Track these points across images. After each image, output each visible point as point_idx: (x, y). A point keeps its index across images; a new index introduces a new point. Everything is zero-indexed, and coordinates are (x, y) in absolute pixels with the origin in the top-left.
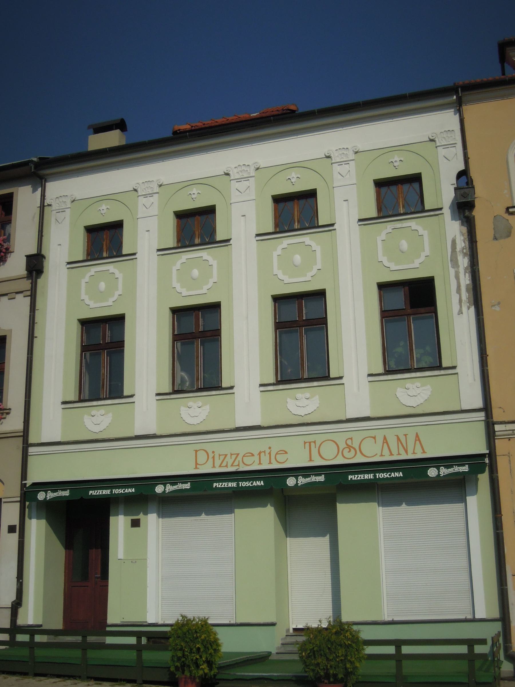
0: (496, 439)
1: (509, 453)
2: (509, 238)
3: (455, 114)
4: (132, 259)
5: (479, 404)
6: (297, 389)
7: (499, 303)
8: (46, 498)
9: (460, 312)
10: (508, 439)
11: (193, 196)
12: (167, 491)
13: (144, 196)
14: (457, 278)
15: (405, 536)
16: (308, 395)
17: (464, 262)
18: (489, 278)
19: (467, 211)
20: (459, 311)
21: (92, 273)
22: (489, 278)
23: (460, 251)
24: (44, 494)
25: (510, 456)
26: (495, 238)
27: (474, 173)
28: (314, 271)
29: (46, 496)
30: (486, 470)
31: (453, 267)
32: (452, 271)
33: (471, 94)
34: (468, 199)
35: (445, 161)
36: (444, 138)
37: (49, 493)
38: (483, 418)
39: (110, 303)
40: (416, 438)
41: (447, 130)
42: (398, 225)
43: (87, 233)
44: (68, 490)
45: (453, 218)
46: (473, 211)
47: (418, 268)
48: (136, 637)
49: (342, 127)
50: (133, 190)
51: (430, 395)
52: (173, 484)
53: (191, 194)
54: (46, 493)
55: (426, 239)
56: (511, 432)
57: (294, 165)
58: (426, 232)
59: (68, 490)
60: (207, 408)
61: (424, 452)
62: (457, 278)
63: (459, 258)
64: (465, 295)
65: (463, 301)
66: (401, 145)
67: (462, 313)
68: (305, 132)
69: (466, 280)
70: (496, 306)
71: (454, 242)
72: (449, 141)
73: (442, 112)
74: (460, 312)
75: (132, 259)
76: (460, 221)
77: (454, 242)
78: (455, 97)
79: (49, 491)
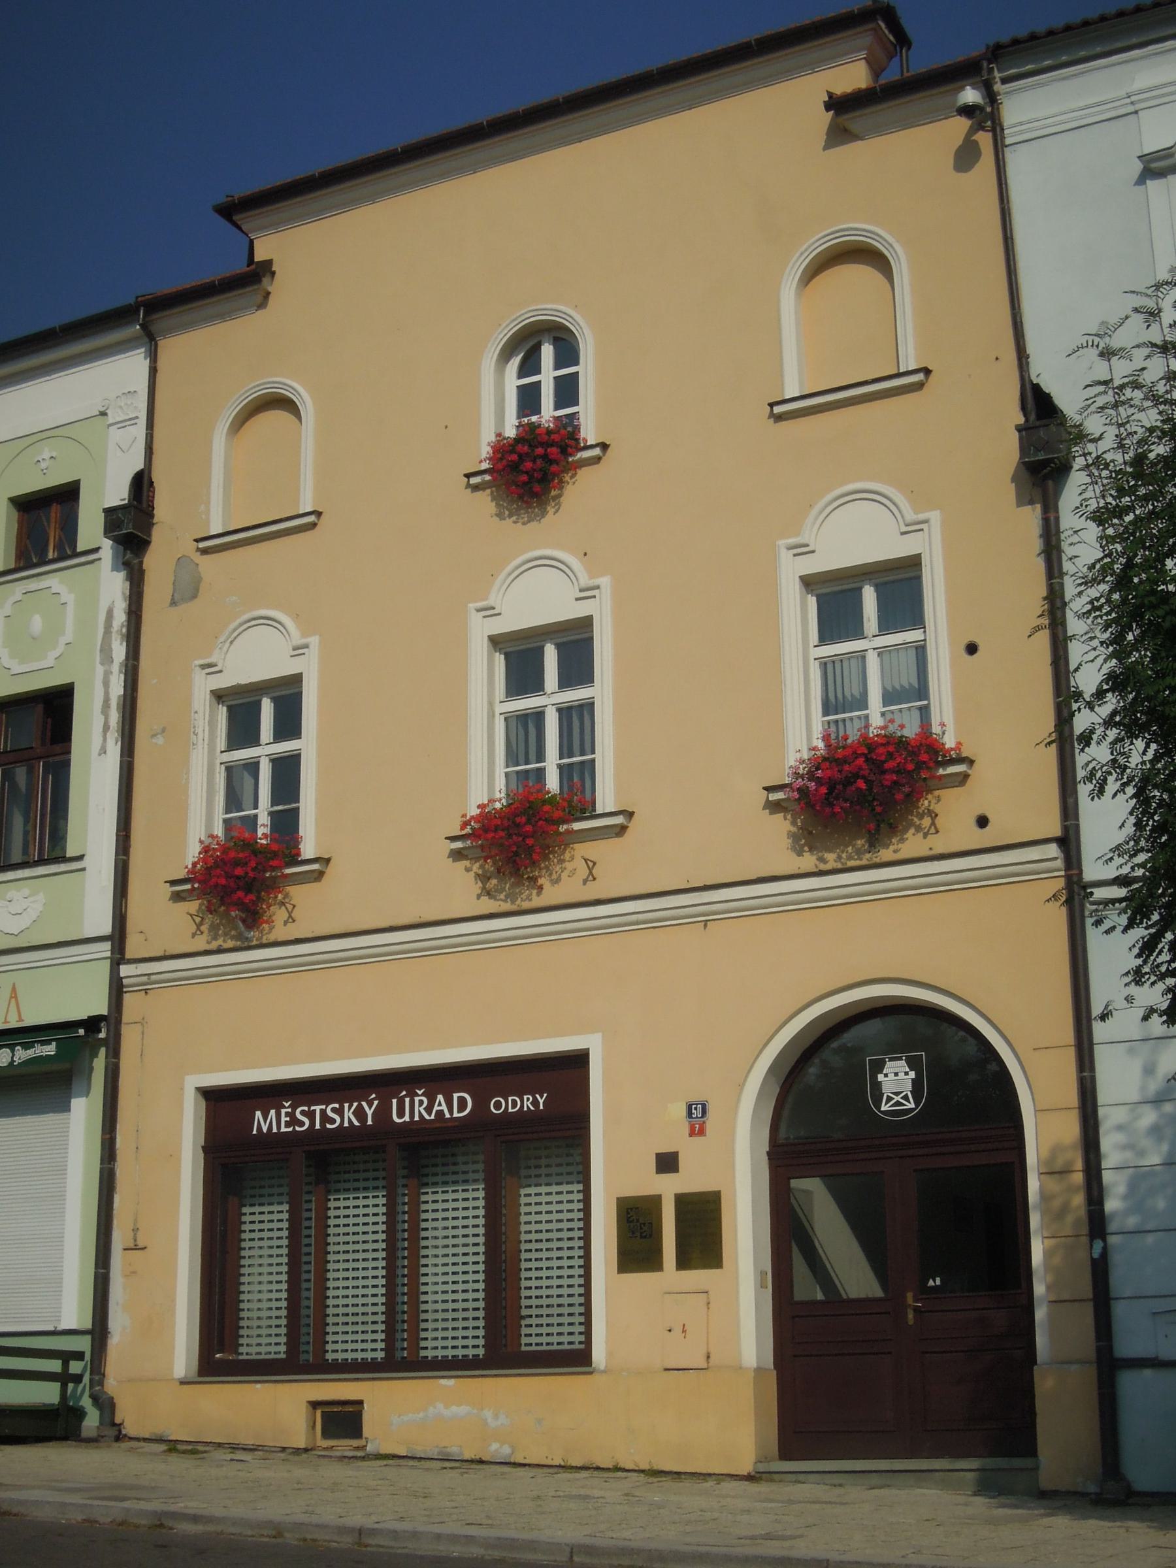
0: (126, 992)
1: (143, 1019)
2: (196, 600)
3: (145, 358)
4: (92, 562)
5: (106, 928)
6: (78, 873)
7: (163, 730)
8: (13, 1061)
9: (103, 751)
10: (144, 992)
11: (43, 465)
12: (17, 1061)
13: (119, 425)
14: (106, 684)
15: (54, 1173)
16: (26, 892)
17: (119, 651)
18: (155, 681)
19: (129, 552)
20: (101, 750)
21: (18, 596)
22: (155, 681)
23: (118, 631)
24: (8, 1054)
25: (145, 1024)
26: (173, 603)
27: (156, 476)
28: (60, 649)
29: (12, 1057)
30: (100, 1055)
31: (102, 664)
32: (100, 670)
33: (192, 308)
34: (122, 530)
35: (119, 453)
36: (121, 407)
37: (18, 1050)
38: (108, 954)
39: (49, 661)
40: (12, 994)
41: (126, 391)
42: (33, 585)
43: (19, 511)
44: (54, 1044)
45: (115, 568)
46: (146, 552)
47: (52, 667)
48: (61, 1361)
49: (48, 373)
50: (98, 413)
51: (41, 912)
52: (27, 1046)
53: (39, 461)
54: (13, 1051)
55: (70, 610)
56: (146, 977)
57: (44, 435)
58: (72, 596)
59: (54, 1044)
60: (41, 897)
61: (21, 1020)
62: (106, 684)
63: (113, 647)
64: (115, 717)
65: (111, 728)
66: (25, 436)
67: (105, 753)
68: (69, 366)
69: (117, 688)
70: (159, 736)
71: (110, 614)
72: (127, 414)
73: (127, 354)
74: (103, 751)
75: (92, 562)
76: (125, 572)
77: (110, 614)
78: (138, 327)
79: (18, 1048)
